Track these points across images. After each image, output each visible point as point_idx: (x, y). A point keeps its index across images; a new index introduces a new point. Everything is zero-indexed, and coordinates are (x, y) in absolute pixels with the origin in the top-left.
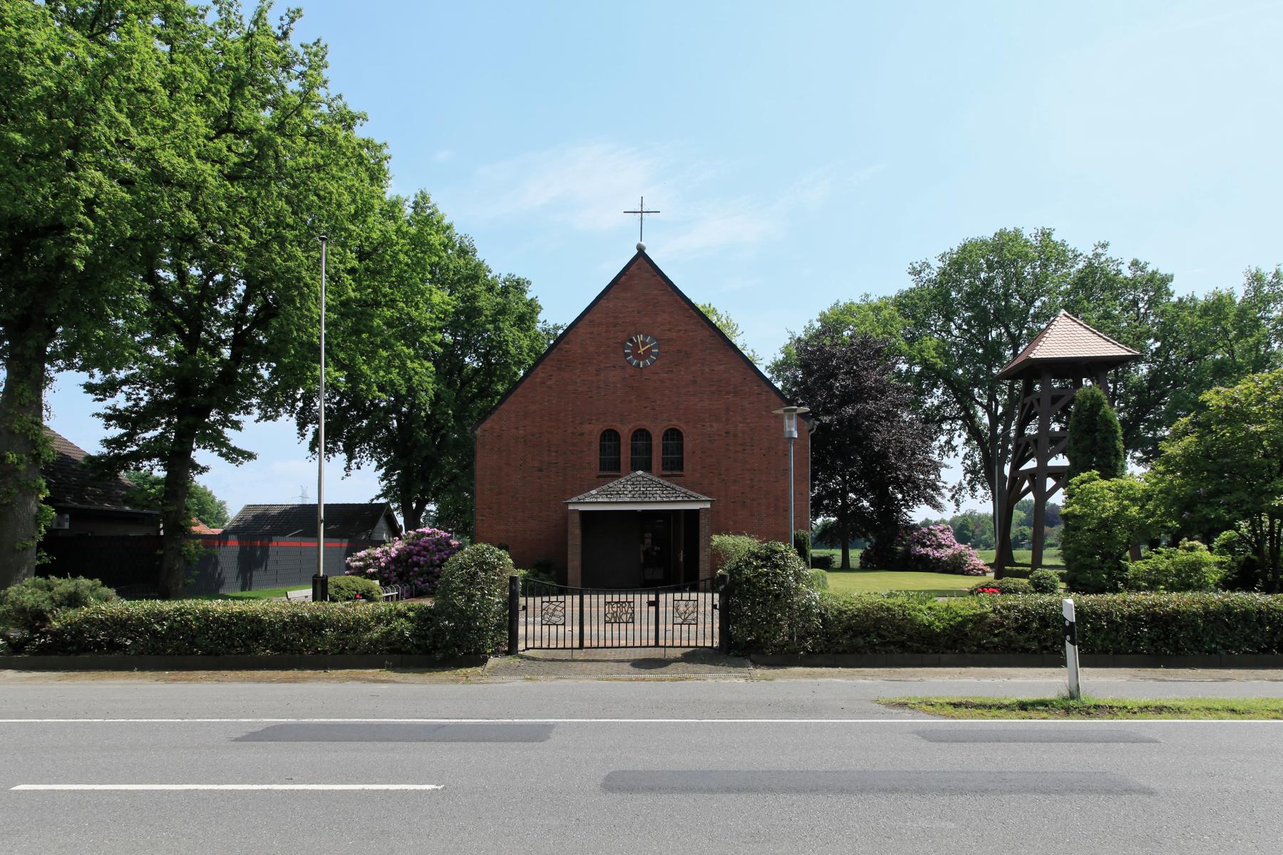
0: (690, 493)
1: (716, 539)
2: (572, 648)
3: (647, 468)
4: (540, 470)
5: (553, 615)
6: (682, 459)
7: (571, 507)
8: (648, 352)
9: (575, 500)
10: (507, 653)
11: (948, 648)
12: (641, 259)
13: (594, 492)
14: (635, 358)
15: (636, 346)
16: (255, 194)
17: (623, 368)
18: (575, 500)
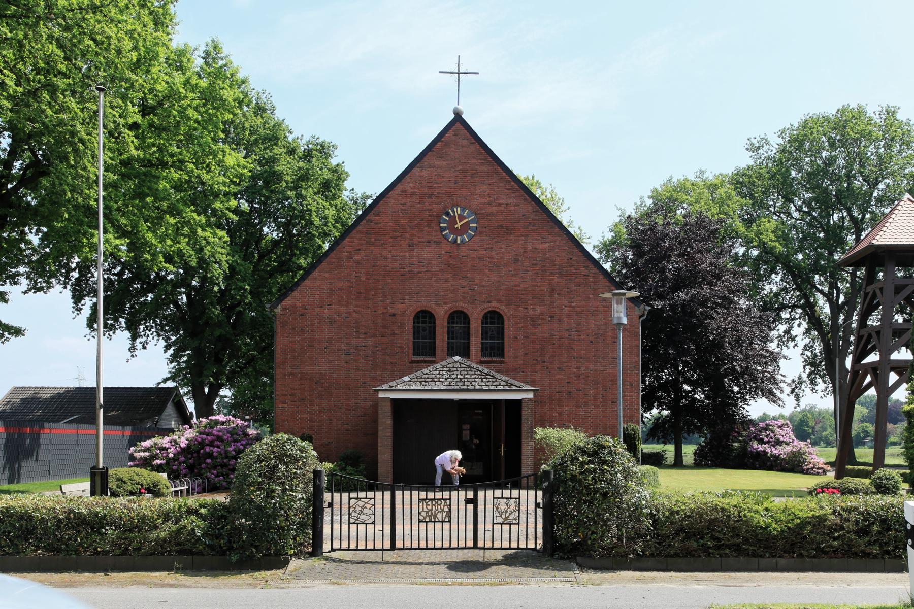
0: (511, 381)
1: (540, 432)
2: (383, 550)
3: (465, 353)
4: (348, 354)
5: (362, 513)
6: (503, 344)
7: (381, 395)
8: (466, 227)
9: (386, 386)
10: (312, 555)
12: (458, 124)
13: (406, 379)
15: (453, 221)
18: (386, 386)
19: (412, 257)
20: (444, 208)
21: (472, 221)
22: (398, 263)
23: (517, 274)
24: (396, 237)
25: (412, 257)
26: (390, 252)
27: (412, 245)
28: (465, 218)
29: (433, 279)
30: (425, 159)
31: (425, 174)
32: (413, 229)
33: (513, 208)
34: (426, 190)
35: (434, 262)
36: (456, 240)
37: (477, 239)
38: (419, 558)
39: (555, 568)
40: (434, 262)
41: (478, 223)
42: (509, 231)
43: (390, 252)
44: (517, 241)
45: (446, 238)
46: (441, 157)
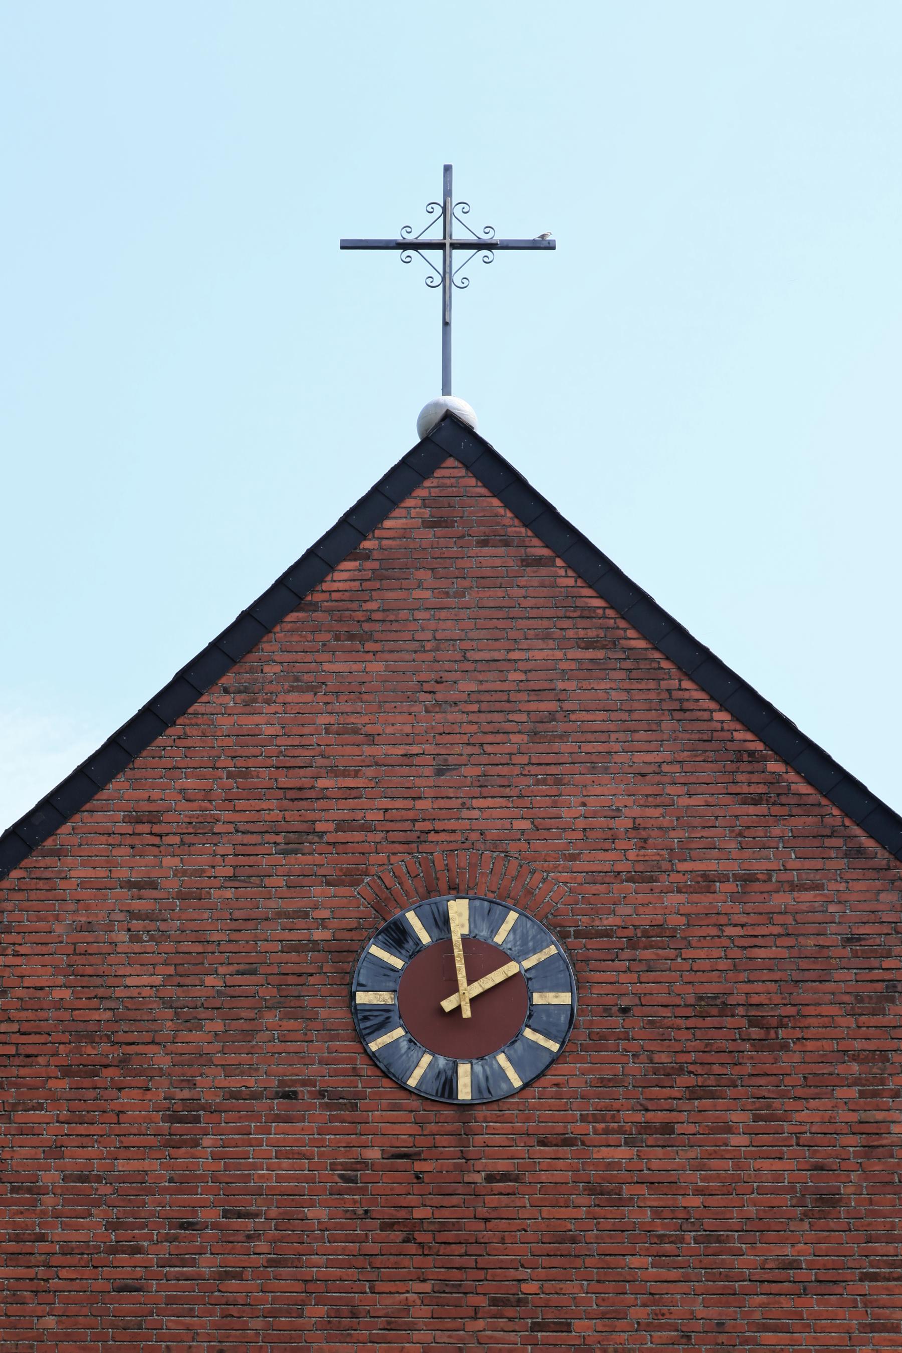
8: (505, 1011)
11: (366, 1164)
12: (451, 473)
14: (419, 1038)
15: (433, 969)
16: (317, 1266)
17: (341, 1102)
19: (184, 1183)
20: (379, 908)
21: (545, 976)
22: (98, 1216)
23: (827, 1285)
24: (91, 1070)
25: (184, 1183)
26: (56, 1151)
27: (185, 1116)
28: (500, 957)
29: (316, 1312)
30: (268, 647)
31: (265, 722)
32: (193, 1023)
33: (782, 900)
34: (271, 809)
35: (317, 1213)
36: (449, 1085)
37: (574, 1074)
38: (553, 655)
39: (463, 418)
40: (317, 1213)
41: (579, 986)
42: (766, 1029)
43: (56, 1151)
44: (819, 1084)
45: (386, 1070)
46: (357, 637)
